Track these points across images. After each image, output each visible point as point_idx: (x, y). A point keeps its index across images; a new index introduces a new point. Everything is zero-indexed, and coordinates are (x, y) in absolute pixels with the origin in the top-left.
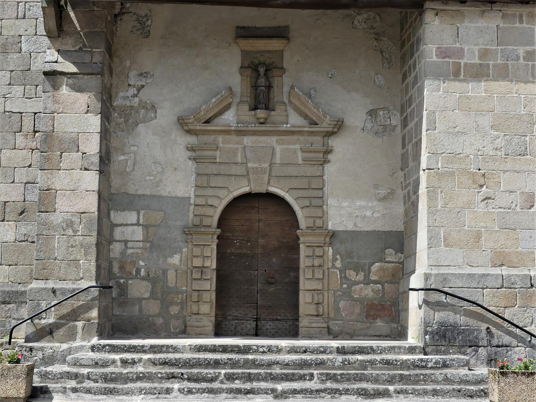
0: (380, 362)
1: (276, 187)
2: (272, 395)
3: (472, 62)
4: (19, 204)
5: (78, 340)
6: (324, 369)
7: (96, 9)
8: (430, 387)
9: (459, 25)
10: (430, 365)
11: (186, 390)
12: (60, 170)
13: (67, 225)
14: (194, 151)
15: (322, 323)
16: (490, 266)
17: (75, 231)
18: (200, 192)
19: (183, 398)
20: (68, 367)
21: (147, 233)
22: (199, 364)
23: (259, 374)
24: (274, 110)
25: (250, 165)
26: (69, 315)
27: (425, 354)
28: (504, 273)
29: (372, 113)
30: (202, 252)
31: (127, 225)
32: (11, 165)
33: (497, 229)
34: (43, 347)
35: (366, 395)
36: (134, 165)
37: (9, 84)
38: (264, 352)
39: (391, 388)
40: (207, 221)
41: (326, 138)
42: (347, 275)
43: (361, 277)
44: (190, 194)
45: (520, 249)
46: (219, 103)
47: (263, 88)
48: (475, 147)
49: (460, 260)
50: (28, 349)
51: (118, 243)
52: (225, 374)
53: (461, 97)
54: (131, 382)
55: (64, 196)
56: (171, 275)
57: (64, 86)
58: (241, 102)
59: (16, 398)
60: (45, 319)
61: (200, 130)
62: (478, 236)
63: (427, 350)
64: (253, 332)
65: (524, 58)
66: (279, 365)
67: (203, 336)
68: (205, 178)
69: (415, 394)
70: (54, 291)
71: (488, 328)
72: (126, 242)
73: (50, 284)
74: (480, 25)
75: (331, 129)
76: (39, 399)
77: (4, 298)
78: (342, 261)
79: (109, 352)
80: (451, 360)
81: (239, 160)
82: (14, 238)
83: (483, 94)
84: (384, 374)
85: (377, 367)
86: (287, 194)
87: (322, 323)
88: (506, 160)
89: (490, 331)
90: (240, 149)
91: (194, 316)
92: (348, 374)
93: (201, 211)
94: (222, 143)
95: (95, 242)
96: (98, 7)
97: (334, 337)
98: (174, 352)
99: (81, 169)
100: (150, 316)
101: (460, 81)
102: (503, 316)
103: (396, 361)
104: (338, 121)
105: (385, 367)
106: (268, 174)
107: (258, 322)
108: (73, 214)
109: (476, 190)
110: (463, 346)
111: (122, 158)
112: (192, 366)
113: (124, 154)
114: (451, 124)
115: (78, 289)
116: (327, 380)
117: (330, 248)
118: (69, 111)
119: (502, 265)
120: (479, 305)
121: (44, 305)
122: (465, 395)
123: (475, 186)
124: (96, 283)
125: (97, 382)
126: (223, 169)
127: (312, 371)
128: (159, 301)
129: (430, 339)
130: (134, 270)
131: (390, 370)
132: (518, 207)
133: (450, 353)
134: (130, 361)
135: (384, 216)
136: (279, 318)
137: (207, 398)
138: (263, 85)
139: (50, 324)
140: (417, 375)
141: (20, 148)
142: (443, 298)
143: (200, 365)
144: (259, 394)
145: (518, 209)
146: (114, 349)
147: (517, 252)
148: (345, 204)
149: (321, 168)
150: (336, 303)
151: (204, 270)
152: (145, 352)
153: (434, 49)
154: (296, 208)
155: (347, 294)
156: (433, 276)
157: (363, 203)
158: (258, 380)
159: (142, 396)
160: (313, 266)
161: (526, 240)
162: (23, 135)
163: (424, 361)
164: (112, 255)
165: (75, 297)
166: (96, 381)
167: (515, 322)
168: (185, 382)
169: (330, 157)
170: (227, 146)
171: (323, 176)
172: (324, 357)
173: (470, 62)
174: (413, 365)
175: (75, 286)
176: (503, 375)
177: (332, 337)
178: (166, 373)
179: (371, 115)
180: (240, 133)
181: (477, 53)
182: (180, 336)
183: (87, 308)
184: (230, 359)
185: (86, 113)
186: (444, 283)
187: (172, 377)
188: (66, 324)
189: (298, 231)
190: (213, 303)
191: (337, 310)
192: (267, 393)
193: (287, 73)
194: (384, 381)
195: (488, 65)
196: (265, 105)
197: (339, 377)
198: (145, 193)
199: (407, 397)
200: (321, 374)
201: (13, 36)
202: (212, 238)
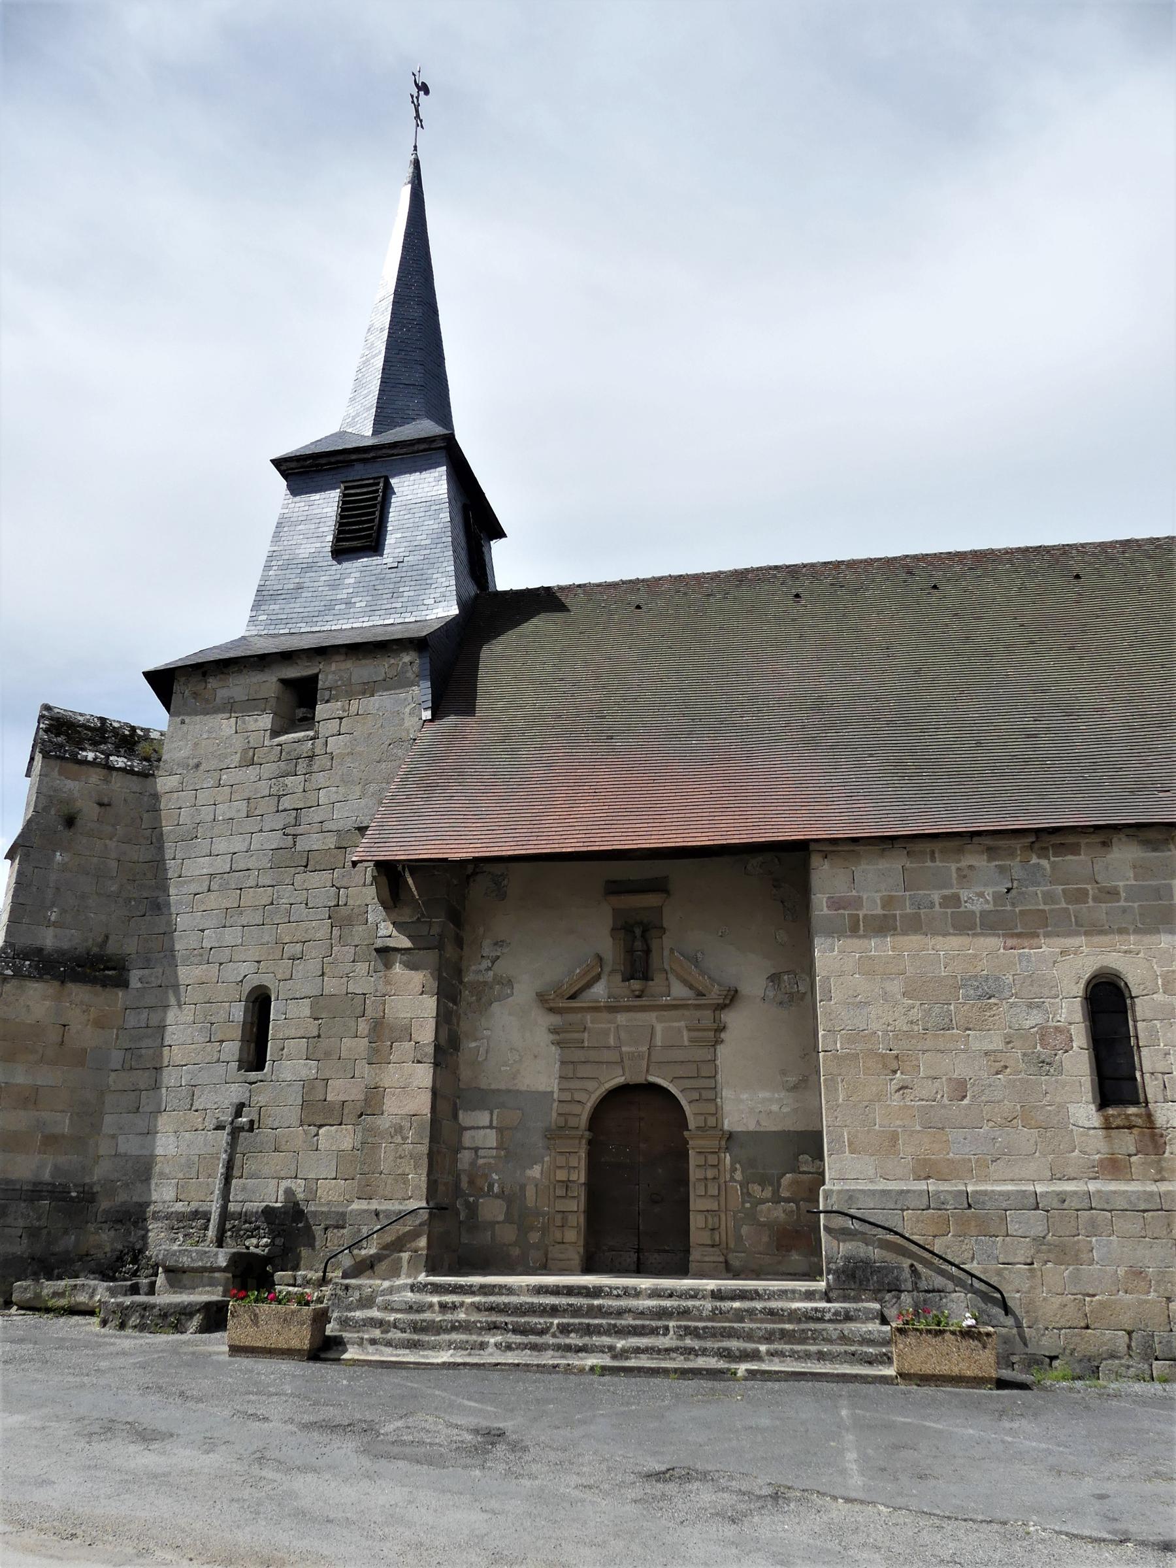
0: (761, 1312)
1: (658, 1077)
2: (609, 1354)
3: (874, 912)
4: (358, 1103)
5: (403, 1276)
6: (689, 1320)
7: (436, 873)
8: (813, 1348)
9: (853, 868)
10: (828, 1316)
11: (504, 1344)
12: (389, 1063)
13: (395, 1131)
14: (558, 1033)
15: (719, 1255)
16: (911, 1179)
17: (405, 1138)
18: (566, 1085)
19: (501, 1355)
20: (378, 1311)
21: (502, 1138)
22: (532, 1310)
23: (601, 1325)
24: (653, 980)
25: (624, 1049)
26: (393, 1244)
27: (829, 1301)
28: (970, 1189)
29: (774, 978)
30: (567, 1162)
31: (478, 1128)
32: (352, 1057)
33: (918, 1128)
34: (361, 1285)
35: (730, 1357)
36: (487, 1053)
37: (353, 962)
38: (618, 1296)
39: (763, 1348)
40: (573, 1122)
41: (717, 1012)
42: (750, 1191)
43: (768, 1193)
44: (553, 1087)
45: (951, 1155)
46: (584, 974)
47: (639, 953)
48: (883, 1021)
49: (871, 1172)
50: (343, 1288)
51: (467, 1151)
52: (558, 1325)
53: (860, 957)
54: (445, 1333)
55: (393, 1095)
56: (530, 1192)
57: (398, 964)
58: (613, 971)
59: (299, 1350)
60: (365, 1249)
61: (563, 1008)
62: (894, 1138)
63: (831, 1295)
64: (634, 1267)
65: (940, 904)
66: (632, 1314)
67: (567, 1273)
68: (571, 1066)
69: (794, 1357)
70: (377, 1214)
71: (912, 1266)
72: (476, 1149)
73: (374, 1205)
74: (880, 867)
75: (721, 1001)
76: (332, 1351)
77: (337, 1221)
78: (743, 1172)
79: (431, 1293)
80: (856, 1310)
81: (612, 1042)
82: (351, 1146)
83: (890, 953)
84: (759, 1329)
85: (757, 1319)
86: (671, 1085)
87: (719, 1255)
88: (925, 1036)
89: (916, 1269)
90: (612, 1029)
91: (557, 1246)
92: (713, 1327)
93: (567, 1108)
94: (591, 1023)
95: (426, 1152)
96: (438, 871)
97: (734, 1276)
98: (508, 1295)
99: (413, 1062)
100: (505, 1245)
101: (860, 937)
102: (931, 1249)
103: (782, 1310)
104: (729, 991)
105: (768, 1319)
106: (646, 1060)
107: (641, 1254)
108: (403, 1117)
109: (888, 1077)
110: (880, 1291)
111: (473, 1045)
112: (524, 1314)
113: (475, 1040)
114: (851, 992)
115: (405, 1211)
116: (686, 1335)
117: (728, 1154)
118: (401, 994)
119: (929, 1177)
120: (896, 1233)
121: (365, 1231)
122: (861, 1360)
123: (886, 1072)
124: (427, 1203)
125: (405, 1332)
126: (593, 1055)
127: (667, 1323)
128: (515, 1226)
129: (834, 1280)
130: (486, 1184)
131: (774, 1322)
132: (945, 1098)
133: (862, 1301)
134: (450, 1305)
135: (795, 1110)
136: (667, 1248)
137: (530, 1356)
138: (640, 948)
139: (371, 1256)
140: (803, 1330)
141: (363, 1036)
142: (849, 1224)
143: (534, 1312)
144: (593, 1352)
145: (946, 1101)
146: (437, 1289)
147: (949, 1160)
148: (744, 1096)
149: (712, 1050)
150: (737, 1228)
151: (570, 1184)
152: (473, 1293)
153: (825, 899)
154: (684, 1103)
155: (751, 1216)
156: (835, 1193)
157: (767, 1095)
158: (599, 1334)
159: (451, 1351)
160: (706, 1179)
161: (959, 1143)
162: (366, 1020)
163: (820, 1311)
164: (460, 1166)
165: (401, 1220)
166: (403, 1331)
167: (949, 1258)
168: (510, 1335)
169: (723, 1035)
170: (596, 1026)
171: (715, 1060)
172: (690, 1303)
173: (871, 913)
174: (806, 1317)
175: (401, 1208)
176: (901, 1334)
177: (730, 1275)
178: (487, 1322)
179: (772, 981)
180: (612, 1009)
181: (879, 901)
182: (539, 1272)
183: (414, 1235)
184: (571, 1305)
185: (421, 994)
186: (850, 1202)
187: (493, 1327)
188: (388, 1256)
189: (686, 1133)
190: (580, 1230)
191: (739, 1238)
192: (603, 1352)
193: (668, 933)
194: (760, 1338)
195: (895, 916)
196: (643, 973)
197: (701, 1331)
198: (500, 1088)
199: (783, 1362)
200: (679, 1327)
201: (359, 906)
202: (580, 1143)
